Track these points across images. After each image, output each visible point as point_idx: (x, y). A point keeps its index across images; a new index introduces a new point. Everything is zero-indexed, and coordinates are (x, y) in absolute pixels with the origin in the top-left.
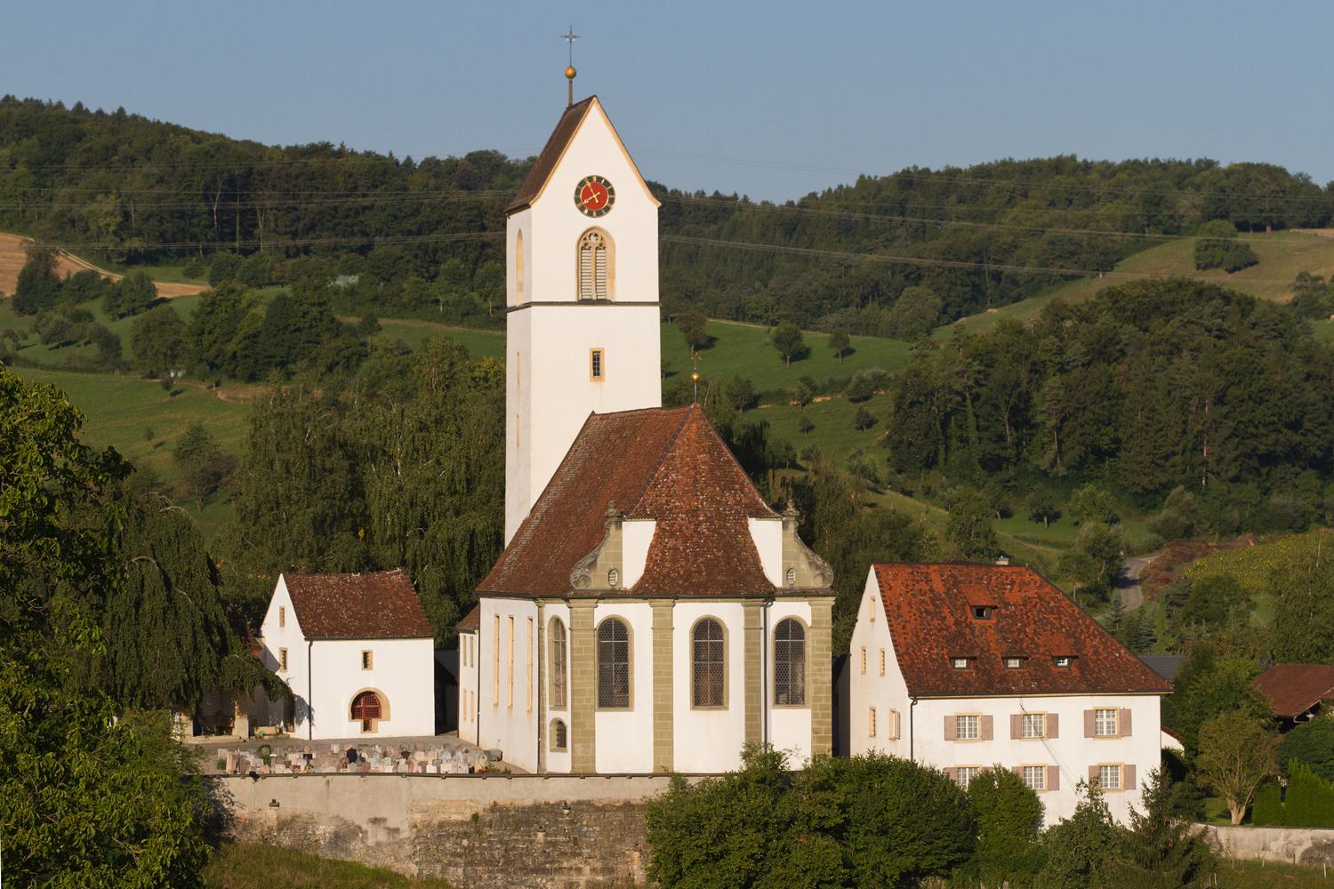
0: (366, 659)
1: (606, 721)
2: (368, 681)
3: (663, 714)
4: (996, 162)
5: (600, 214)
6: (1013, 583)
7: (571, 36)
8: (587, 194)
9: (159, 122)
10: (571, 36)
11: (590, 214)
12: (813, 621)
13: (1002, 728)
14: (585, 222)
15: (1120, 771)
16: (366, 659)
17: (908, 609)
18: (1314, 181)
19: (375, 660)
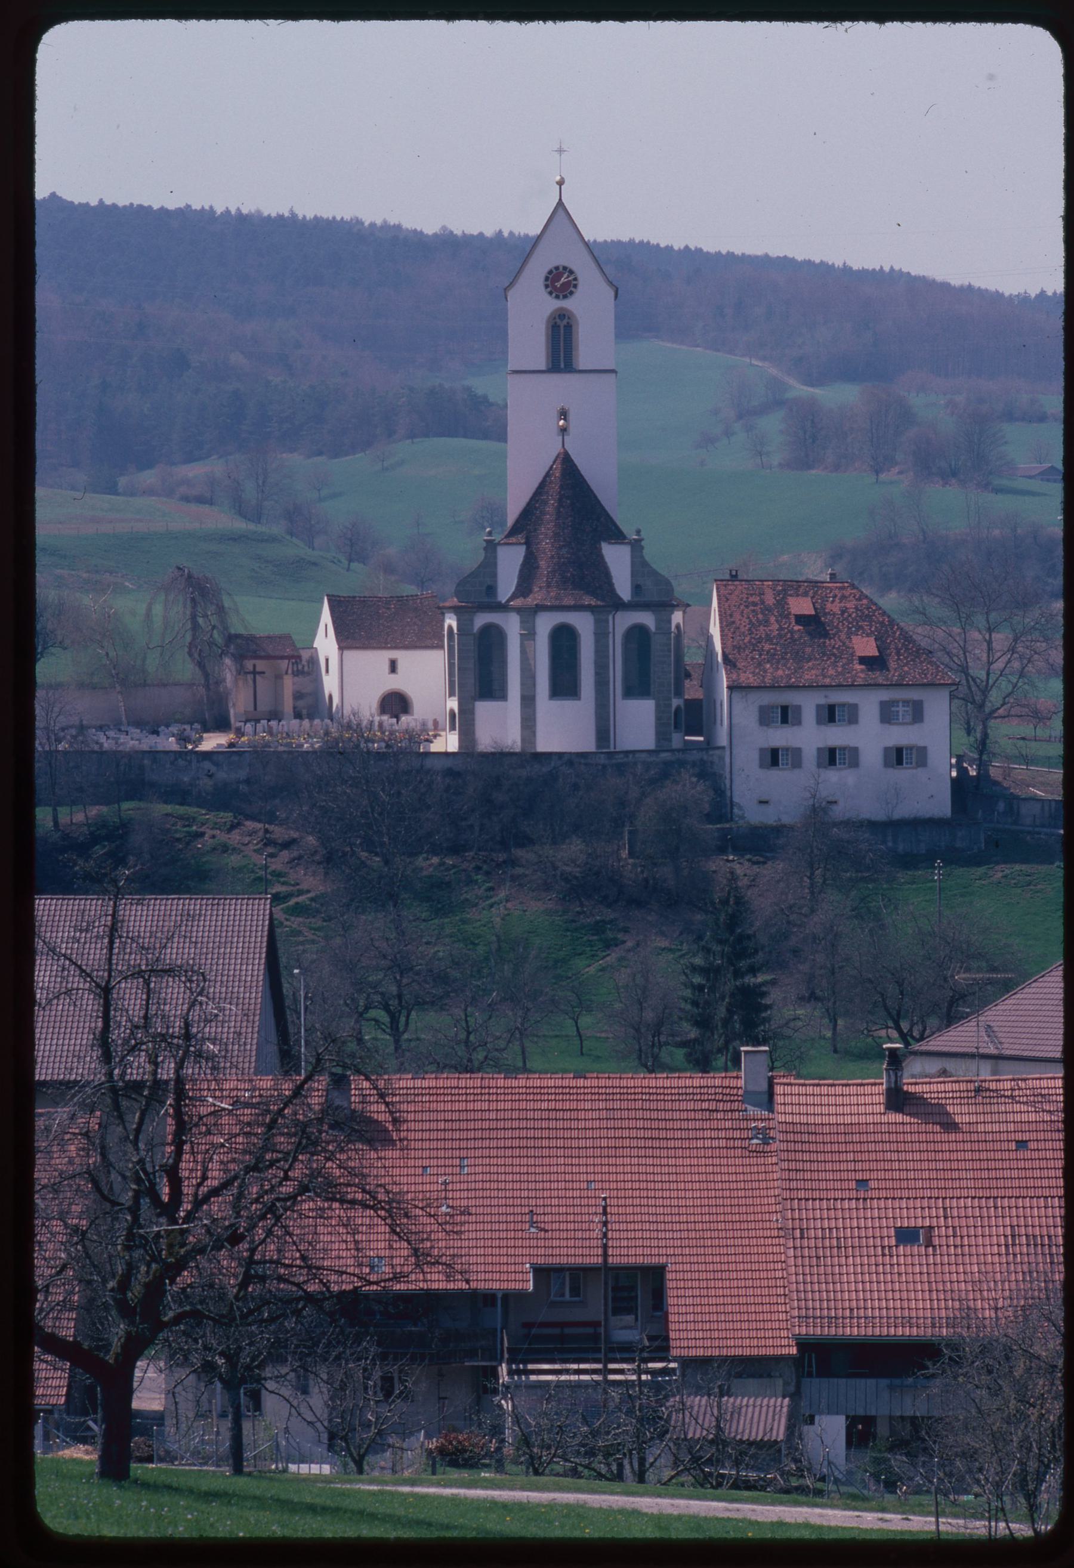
0: (393, 667)
1: (484, 709)
2: (394, 683)
3: (528, 701)
4: (511, 233)
5: (565, 297)
6: (835, 596)
7: (560, 151)
8: (567, 285)
9: (648, 243)
10: (560, 151)
11: (557, 297)
12: (657, 629)
13: (809, 715)
14: (554, 304)
15: (914, 751)
16: (393, 667)
17: (739, 617)
18: (426, 231)
19: (400, 666)
